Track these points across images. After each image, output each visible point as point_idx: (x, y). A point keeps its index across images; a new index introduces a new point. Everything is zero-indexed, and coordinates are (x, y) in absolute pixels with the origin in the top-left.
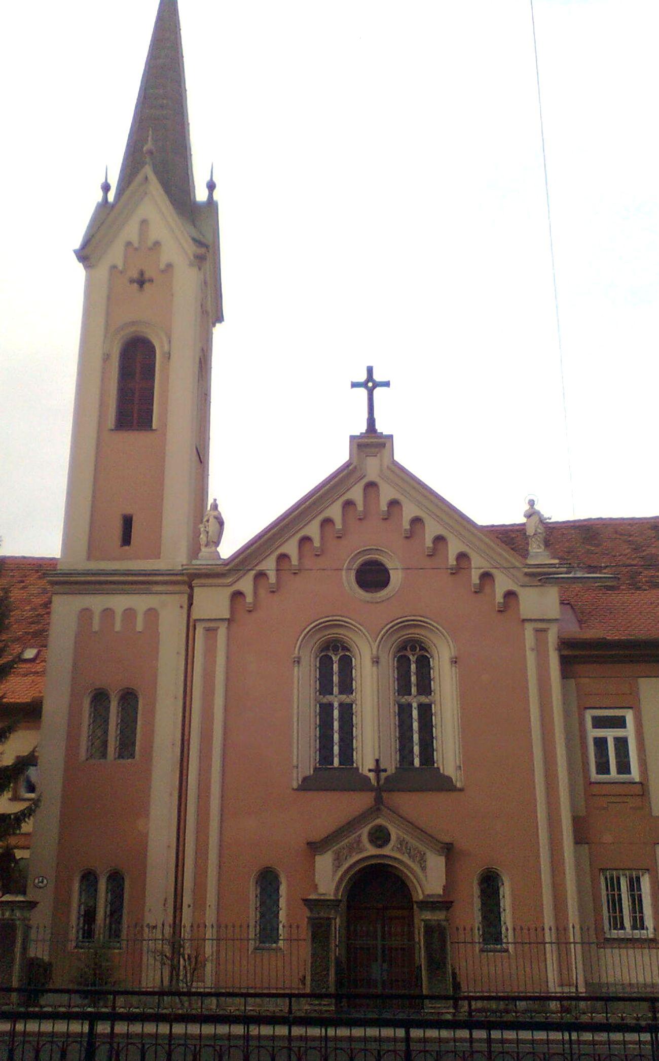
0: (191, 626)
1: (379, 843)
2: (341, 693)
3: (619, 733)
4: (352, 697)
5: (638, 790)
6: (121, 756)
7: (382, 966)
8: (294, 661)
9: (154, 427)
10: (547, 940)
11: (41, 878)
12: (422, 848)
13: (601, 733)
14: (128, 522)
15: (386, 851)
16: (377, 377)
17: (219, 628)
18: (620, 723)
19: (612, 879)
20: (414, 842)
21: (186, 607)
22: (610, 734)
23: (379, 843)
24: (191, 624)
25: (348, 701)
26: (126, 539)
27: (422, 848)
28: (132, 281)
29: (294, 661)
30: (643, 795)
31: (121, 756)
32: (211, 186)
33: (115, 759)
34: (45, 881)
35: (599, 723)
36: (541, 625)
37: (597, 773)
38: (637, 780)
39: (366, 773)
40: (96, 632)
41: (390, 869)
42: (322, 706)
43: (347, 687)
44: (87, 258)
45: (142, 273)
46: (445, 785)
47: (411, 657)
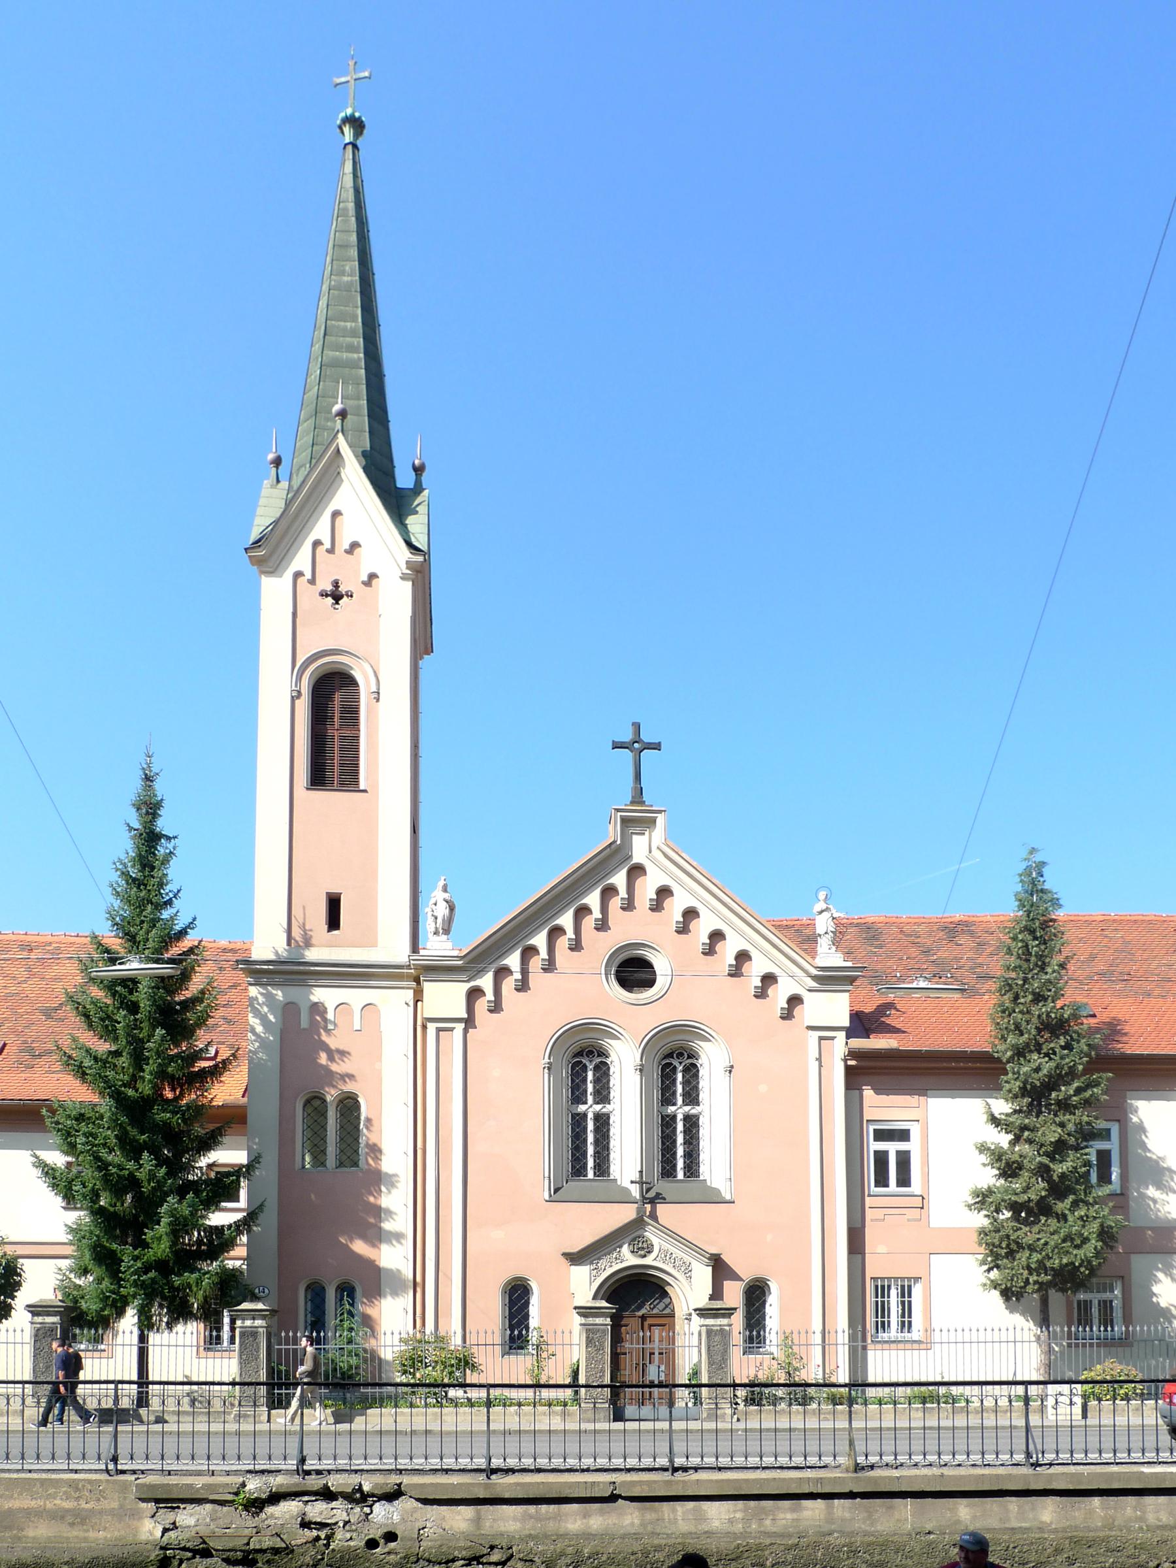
0: (420, 1026)
1: (642, 1253)
2: (685, 1104)
3: (902, 1146)
4: (608, 1108)
5: (917, 1202)
6: (341, 1164)
7: (659, 1367)
8: (544, 1068)
9: (362, 787)
10: (840, 1341)
11: (261, 1288)
12: (687, 1259)
13: (882, 1146)
14: (334, 903)
15: (648, 1261)
16: (627, 736)
17: (454, 1028)
18: (904, 1135)
19: (883, 1287)
20: (678, 1253)
21: (412, 1003)
22: (892, 1148)
23: (642, 1253)
24: (419, 1022)
25: (693, 1112)
26: (334, 922)
27: (687, 1259)
28: (324, 594)
29: (544, 1068)
30: (922, 1208)
31: (341, 1164)
32: (419, 470)
33: (337, 1168)
34: (266, 1291)
35: (880, 1135)
36: (825, 1031)
37: (238, 1201)
38: (918, 1192)
39: (626, 1184)
40: (304, 1029)
41: (653, 1280)
42: (574, 1116)
43: (603, 1095)
44: (337, 583)
45: (336, 584)
46: (712, 1198)
47: (588, 1064)
